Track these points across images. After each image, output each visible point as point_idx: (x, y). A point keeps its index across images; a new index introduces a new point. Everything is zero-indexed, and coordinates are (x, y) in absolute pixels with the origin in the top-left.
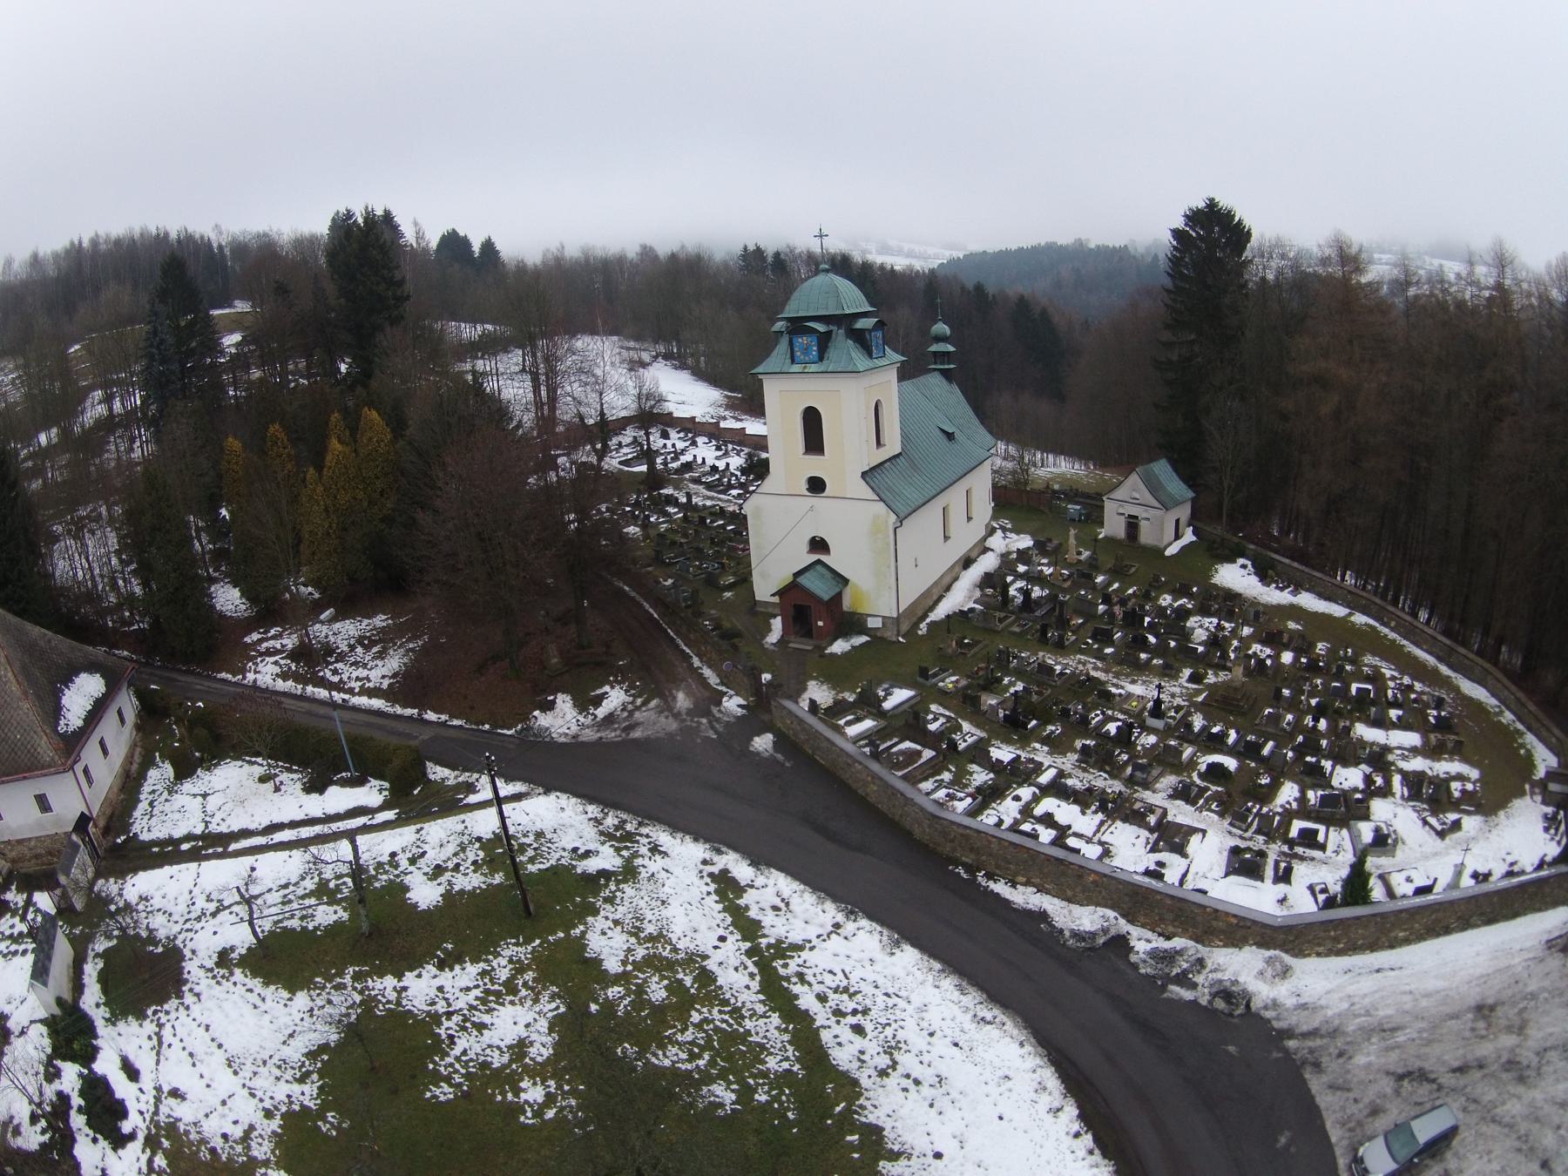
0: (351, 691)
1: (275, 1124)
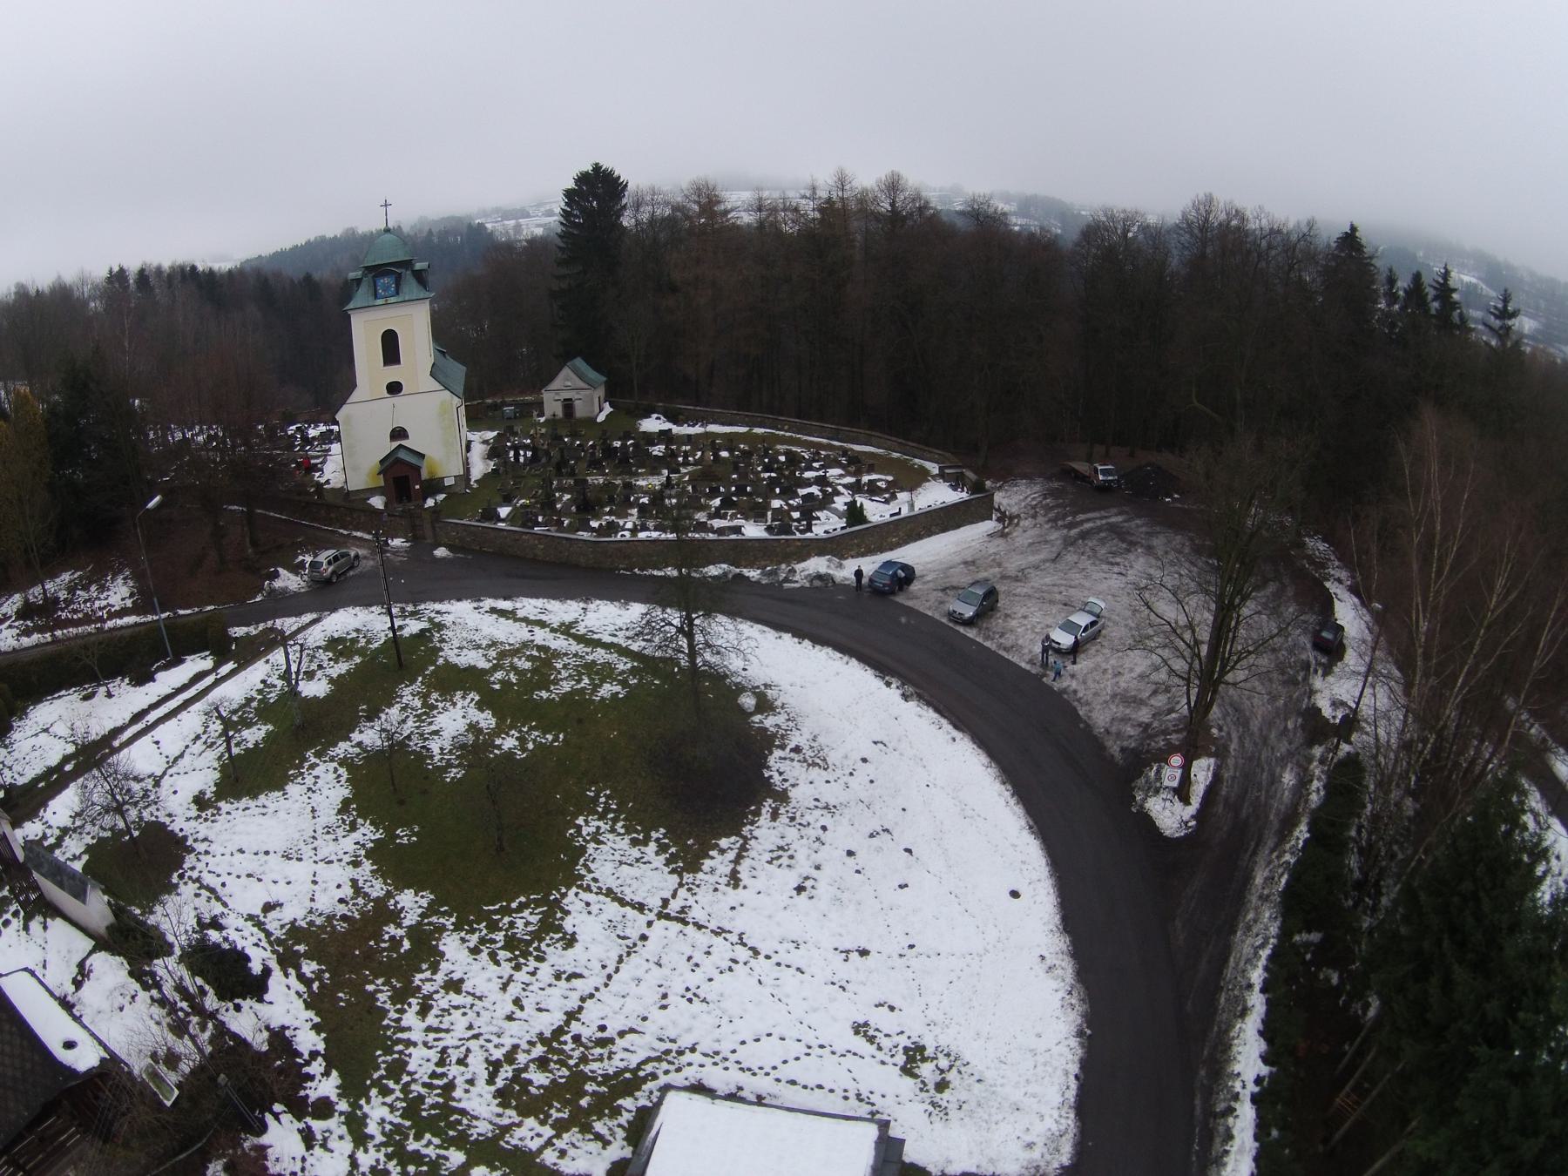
0: (101, 620)
1: (368, 866)
